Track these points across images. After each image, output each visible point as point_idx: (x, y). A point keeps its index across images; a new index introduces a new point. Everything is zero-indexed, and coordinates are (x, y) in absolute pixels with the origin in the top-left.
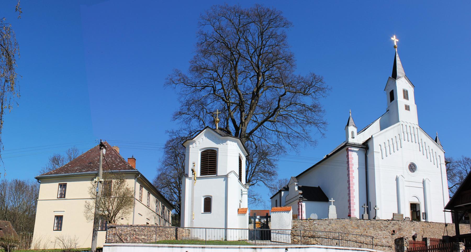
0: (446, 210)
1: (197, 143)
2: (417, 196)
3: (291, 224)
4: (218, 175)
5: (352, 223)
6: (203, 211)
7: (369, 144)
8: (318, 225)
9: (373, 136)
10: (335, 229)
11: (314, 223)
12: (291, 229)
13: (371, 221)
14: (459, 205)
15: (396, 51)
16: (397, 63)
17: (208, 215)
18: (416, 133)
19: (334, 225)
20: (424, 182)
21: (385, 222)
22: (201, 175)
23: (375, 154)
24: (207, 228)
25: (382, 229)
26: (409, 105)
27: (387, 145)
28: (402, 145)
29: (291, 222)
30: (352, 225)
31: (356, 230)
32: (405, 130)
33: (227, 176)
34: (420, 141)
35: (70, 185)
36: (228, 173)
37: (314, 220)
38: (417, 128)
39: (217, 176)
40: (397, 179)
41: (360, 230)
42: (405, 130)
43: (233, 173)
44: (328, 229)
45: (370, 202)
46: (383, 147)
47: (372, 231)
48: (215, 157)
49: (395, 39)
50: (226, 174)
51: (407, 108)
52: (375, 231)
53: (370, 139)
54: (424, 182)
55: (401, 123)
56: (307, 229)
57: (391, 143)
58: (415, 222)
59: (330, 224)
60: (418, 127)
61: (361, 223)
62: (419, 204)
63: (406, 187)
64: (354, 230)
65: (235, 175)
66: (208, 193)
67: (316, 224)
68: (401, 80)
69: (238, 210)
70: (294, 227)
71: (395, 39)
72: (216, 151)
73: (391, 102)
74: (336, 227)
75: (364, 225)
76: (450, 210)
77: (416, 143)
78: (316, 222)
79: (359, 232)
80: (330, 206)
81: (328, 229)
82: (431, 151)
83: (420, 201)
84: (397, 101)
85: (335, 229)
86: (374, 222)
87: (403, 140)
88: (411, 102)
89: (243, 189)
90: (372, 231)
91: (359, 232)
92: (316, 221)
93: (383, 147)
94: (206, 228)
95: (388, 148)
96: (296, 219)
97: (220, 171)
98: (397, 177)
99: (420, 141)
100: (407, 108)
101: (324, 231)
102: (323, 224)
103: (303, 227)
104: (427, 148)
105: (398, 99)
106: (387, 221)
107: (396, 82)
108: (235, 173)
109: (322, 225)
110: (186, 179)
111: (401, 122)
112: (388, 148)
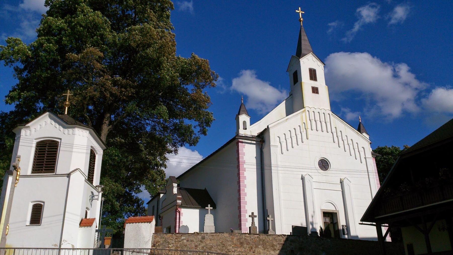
0: (364, 223)
1: (32, 129)
2: (332, 202)
3: (151, 239)
4: (57, 173)
5: (233, 239)
6: (28, 223)
7: (266, 136)
8: (188, 241)
9: (269, 127)
10: (210, 247)
11: (182, 238)
12: (150, 248)
13: (259, 236)
14: (381, 215)
15: (302, 25)
16: (302, 38)
17: (35, 228)
18: (328, 120)
19: (208, 242)
20: (341, 182)
21: (279, 238)
22: (32, 173)
23: (272, 149)
24: (17, 248)
25: (276, 248)
26: (317, 87)
27: (288, 136)
28: (309, 136)
29: (151, 237)
30: (233, 242)
31: (239, 250)
32: (312, 117)
33: (69, 175)
34: (334, 130)
35: (290, 234)
36: (71, 170)
37: (182, 234)
38: (329, 114)
39: (56, 174)
40: (303, 179)
41: (244, 249)
42: (312, 117)
43: (79, 171)
44: (200, 246)
45: (267, 210)
46: (283, 139)
47: (261, 250)
48: (56, 150)
49: (300, 11)
50: (68, 172)
51: (315, 90)
52: (266, 250)
53: (265, 130)
54: (341, 182)
55: (307, 109)
56: (172, 247)
57: (293, 134)
58: (325, 238)
59: (203, 240)
60: (331, 113)
61: (245, 239)
62: (336, 213)
63: (314, 189)
64: (236, 249)
65: (84, 176)
66: (38, 198)
67: (185, 239)
68: (306, 58)
69: (82, 220)
70: (155, 245)
71: (300, 11)
72: (58, 142)
73: (294, 85)
74: (211, 244)
75: (250, 242)
76: (375, 223)
77: (327, 132)
78: (185, 238)
79: (243, 252)
80: (206, 215)
81: (200, 246)
82: (350, 142)
83: (337, 210)
84: (301, 83)
85: (210, 247)
86: (264, 238)
87: (309, 131)
88: (321, 83)
89: (95, 193)
90: (261, 250)
91: (243, 252)
92: (185, 236)
93: (283, 139)
94: (15, 249)
95: (289, 141)
96: (158, 233)
97: (61, 167)
98: (303, 177)
99: (334, 130)
100: (315, 90)
101: (194, 250)
102: (194, 240)
103: (168, 244)
104: (345, 138)
105: (303, 80)
106: (282, 237)
107: (299, 62)
108: (81, 171)
109: (192, 241)
110: (9, 177)
111: (306, 108)
112: (289, 141)
